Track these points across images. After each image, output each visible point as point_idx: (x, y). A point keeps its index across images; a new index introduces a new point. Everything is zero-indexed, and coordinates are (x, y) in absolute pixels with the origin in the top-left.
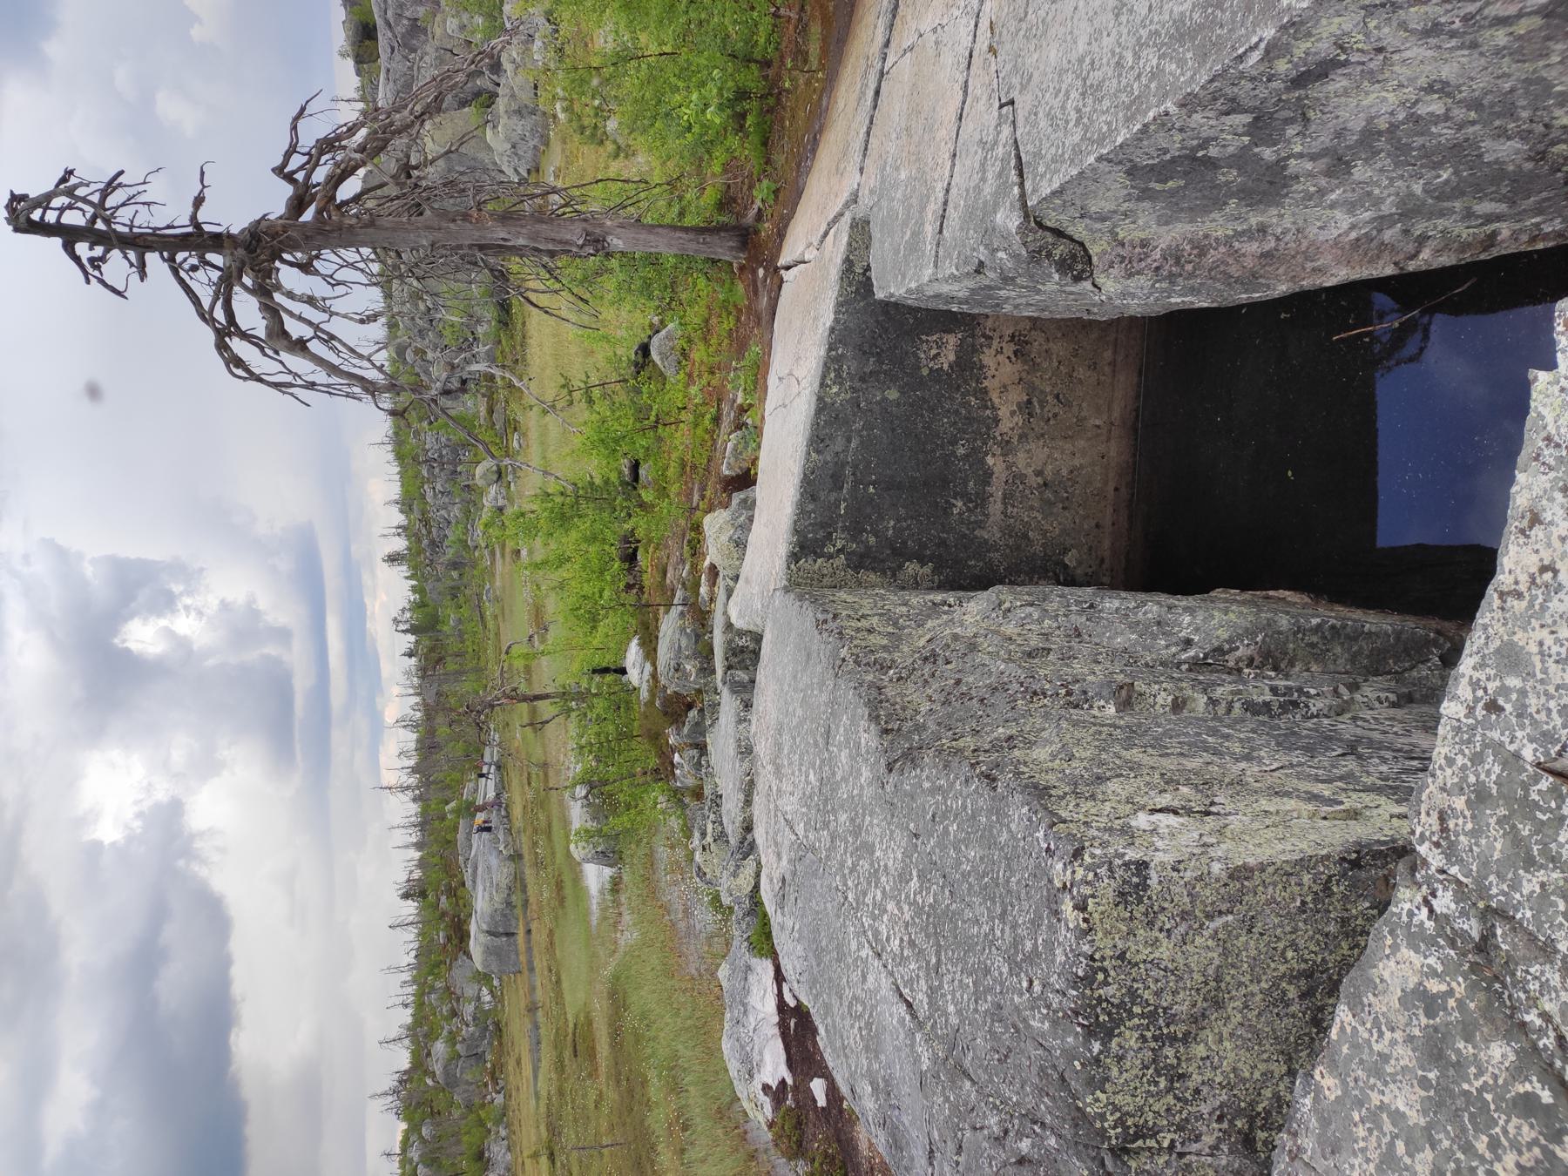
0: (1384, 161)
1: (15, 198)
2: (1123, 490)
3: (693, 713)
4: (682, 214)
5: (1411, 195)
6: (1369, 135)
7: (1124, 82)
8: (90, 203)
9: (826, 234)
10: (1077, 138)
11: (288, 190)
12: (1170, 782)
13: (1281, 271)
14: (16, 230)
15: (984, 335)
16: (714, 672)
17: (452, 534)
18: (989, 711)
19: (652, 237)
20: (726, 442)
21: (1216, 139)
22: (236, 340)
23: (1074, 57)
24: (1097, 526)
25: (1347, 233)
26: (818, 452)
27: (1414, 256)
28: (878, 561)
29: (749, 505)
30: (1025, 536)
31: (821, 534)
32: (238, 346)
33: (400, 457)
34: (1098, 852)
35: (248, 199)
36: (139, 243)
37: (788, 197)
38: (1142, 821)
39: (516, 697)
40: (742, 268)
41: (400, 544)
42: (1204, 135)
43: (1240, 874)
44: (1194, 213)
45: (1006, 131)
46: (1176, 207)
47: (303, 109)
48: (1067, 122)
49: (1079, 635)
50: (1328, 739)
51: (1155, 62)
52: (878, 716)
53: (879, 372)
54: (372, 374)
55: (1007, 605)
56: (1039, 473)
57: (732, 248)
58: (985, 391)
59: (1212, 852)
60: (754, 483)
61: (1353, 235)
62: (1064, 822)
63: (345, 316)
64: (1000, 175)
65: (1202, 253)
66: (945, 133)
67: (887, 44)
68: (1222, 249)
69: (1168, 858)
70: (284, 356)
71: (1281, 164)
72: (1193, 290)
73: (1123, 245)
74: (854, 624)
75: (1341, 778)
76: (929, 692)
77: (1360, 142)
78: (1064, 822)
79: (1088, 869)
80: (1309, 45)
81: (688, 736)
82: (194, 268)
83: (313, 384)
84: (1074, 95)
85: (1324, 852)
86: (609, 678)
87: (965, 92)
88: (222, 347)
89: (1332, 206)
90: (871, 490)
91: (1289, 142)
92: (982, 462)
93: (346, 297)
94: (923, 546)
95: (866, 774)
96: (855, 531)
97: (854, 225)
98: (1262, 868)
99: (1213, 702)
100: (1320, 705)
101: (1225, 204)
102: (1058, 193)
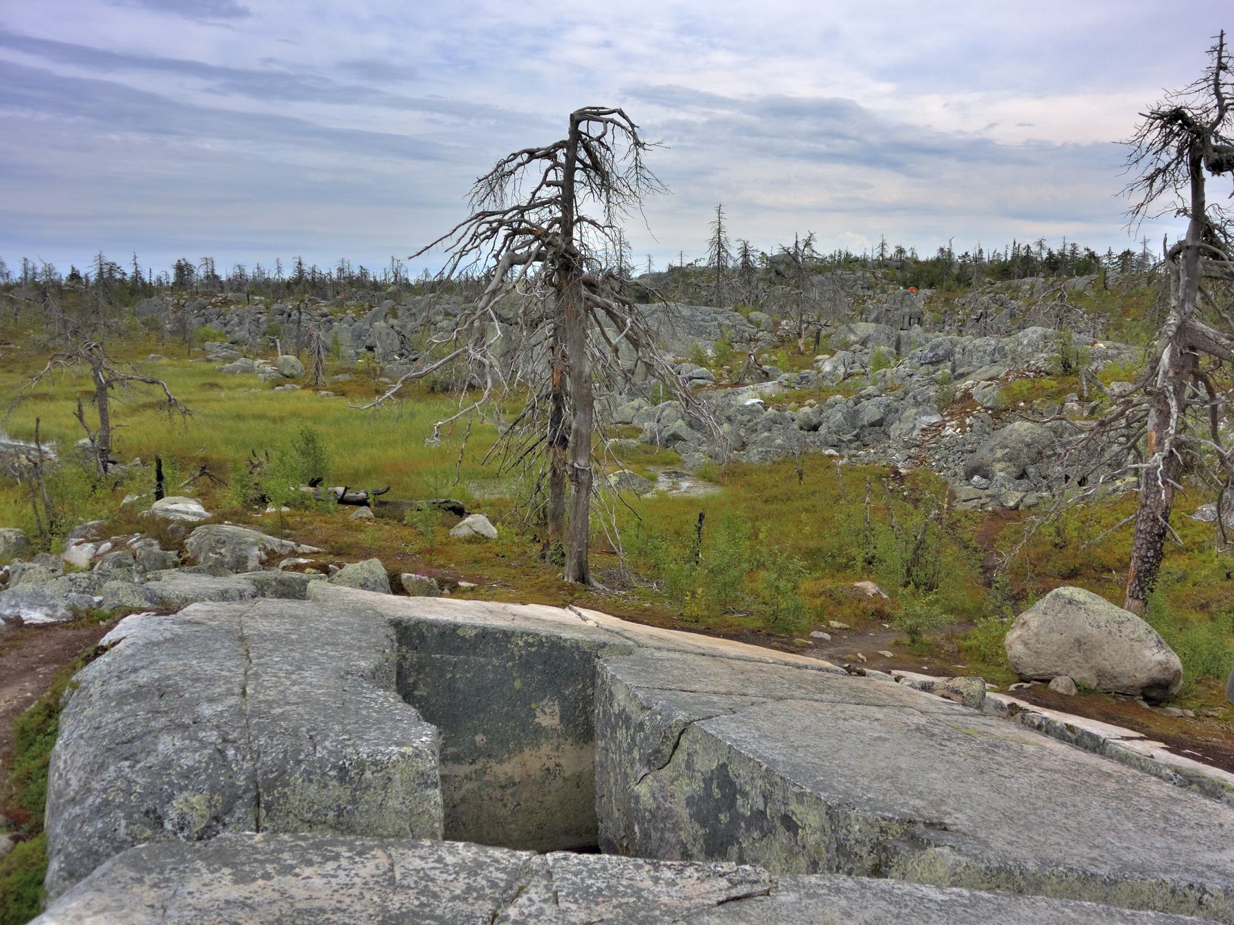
96: (420, 667)
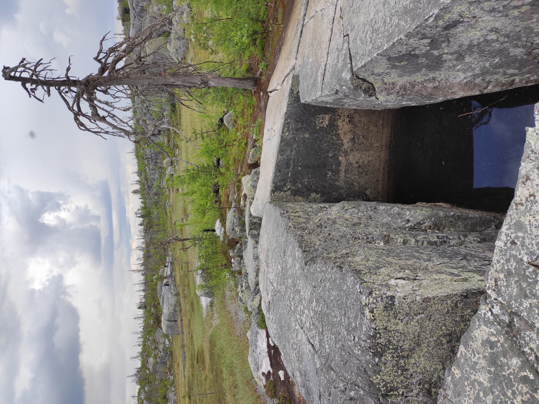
0: (476, 55)
1: (5, 68)
2: (386, 168)
3: (238, 245)
4: (234, 74)
5: (485, 67)
6: (471, 46)
7: (386, 28)
8: (31, 70)
9: (284, 80)
10: (370, 47)
11: (99, 65)
12: (402, 269)
13: (440, 93)
14: (6, 79)
15: (338, 115)
16: (245, 231)
17: (156, 184)
18: (340, 244)
19: (224, 82)
20: (249, 152)
21: (418, 48)
22: (81, 117)
23: (369, 19)
24: (377, 181)
25: (463, 80)
26: (281, 155)
27: (486, 88)
28: (302, 193)
29: (257, 173)
30: (352, 184)
31: (282, 184)
32: (82, 119)
33: (137, 157)
34: (377, 293)
35: (85, 68)
36: (48, 84)
37: (271, 68)
38: (393, 282)
39: (177, 239)
40: (255, 92)
41: (137, 187)
42: (414, 46)
43: (426, 300)
44: (411, 73)
45: (346, 45)
46: (404, 71)
47: (104, 38)
48: (367, 42)
49: (371, 218)
50: (457, 254)
51: (397, 21)
52: (302, 246)
53: (302, 128)
54: (128, 129)
55: (346, 208)
56: (357, 163)
57: (251, 85)
58: (339, 134)
59: (417, 293)
60: (259, 166)
61: (465, 81)
62: (366, 282)
63: (119, 109)
64: (344, 60)
65: (413, 87)
66: (325, 46)
67: (305, 15)
68: (420, 86)
69: (402, 295)
70: (98, 122)
71: (440, 56)
72: (410, 100)
73: (386, 84)
74: (293, 214)
75: (461, 267)
76: (319, 238)
77: (468, 49)
78: (366, 282)
79: (374, 298)
80: (450, 15)
81: (237, 253)
82: (67, 92)
83: (108, 132)
84: (369, 33)
85: (455, 293)
86: (209, 233)
87: (332, 32)
88: (76, 119)
89: (458, 71)
90: (300, 168)
91: (443, 49)
92: (338, 159)
93: (119, 102)
94: (317, 188)
95: (298, 266)
96: (294, 183)
97: (294, 77)
98: (434, 298)
99: (417, 241)
100: (454, 242)
101: (421, 70)
102: (364, 66)
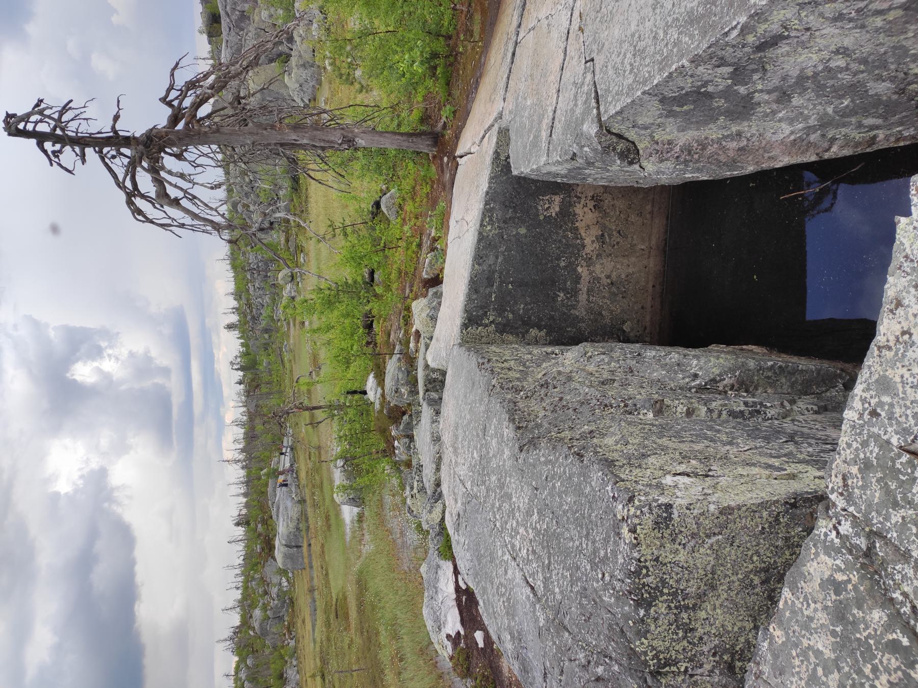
0: (810, 94)
1: (9, 116)
2: (658, 287)
3: (406, 417)
4: (399, 125)
5: (826, 114)
6: (802, 79)
7: (658, 48)
8: (53, 119)
9: (484, 137)
10: (630, 81)
11: (168, 111)
12: (685, 458)
13: (750, 158)
14: (10, 134)
15: (576, 196)
16: (418, 393)
17: (265, 313)
18: (579, 416)
19: (382, 139)
20: (425, 259)
21: (712, 81)
22: (138, 199)
23: (629, 33)
24: (642, 308)
25: (788, 136)
26: (479, 264)
27: (828, 150)
28: (514, 328)
29: (438, 295)
30: (600, 314)
31: (481, 313)
32: (139, 202)
33: (234, 267)
34: (643, 498)
35: (145, 116)
36: (81, 142)
37: (462, 115)
38: (668, 480)
39: (302, 408)
40: (434, 157)
41: (234, 318)
42: (705, 79)
43: (726, 511)
44: (699, 124)
45: (589, 76)
46: (688, 121)
47: (177, 64)
48: (625, 71)
49: (632, 372)
50: (778, 432)
51: (676, 36)
52: (514, 419)
53: (515, 218)
54: (218, 219)
55: (590, 354)
56: (608, 277)
57: (428, 145)
58: (577, 229)
59: (710, 499)
60: (441, 282)
61: (792, 137)
62: (623, 481)
63: (202, 185)
64: (585, 102)
65: (704, 148)
66: (553, 78)
67: (519, 26)
68: (715, 146)
69: (684, 502)
70: (166, 208)
71: (750, 96)
72: (698, 170)
73: (657, 143)
74: (500, 365)
75: (785, 455)
76: (544, 405)
77: (796, 83)
78: (623, 481)
79: (637, 508)
80: (766, 26)
81: (403, 431)
82: (114, 157)
83: (184, 225)
84: (629, 55)
85: (775, 499)
86: (357, 397)
87: (565, 54)
88: (130, 203)
89: (780, 121)
90: (510, 286)
91: (754, 83)
92: (575, 270)
93: (202, 174)
94: (541, 320)
95: (507, 453)
96: (501, 311)
97: (500, 132)
98: (739, 508)
99: (710, 411)
100: (773, 412)
101: (717, 119)
102: (620, 113)
